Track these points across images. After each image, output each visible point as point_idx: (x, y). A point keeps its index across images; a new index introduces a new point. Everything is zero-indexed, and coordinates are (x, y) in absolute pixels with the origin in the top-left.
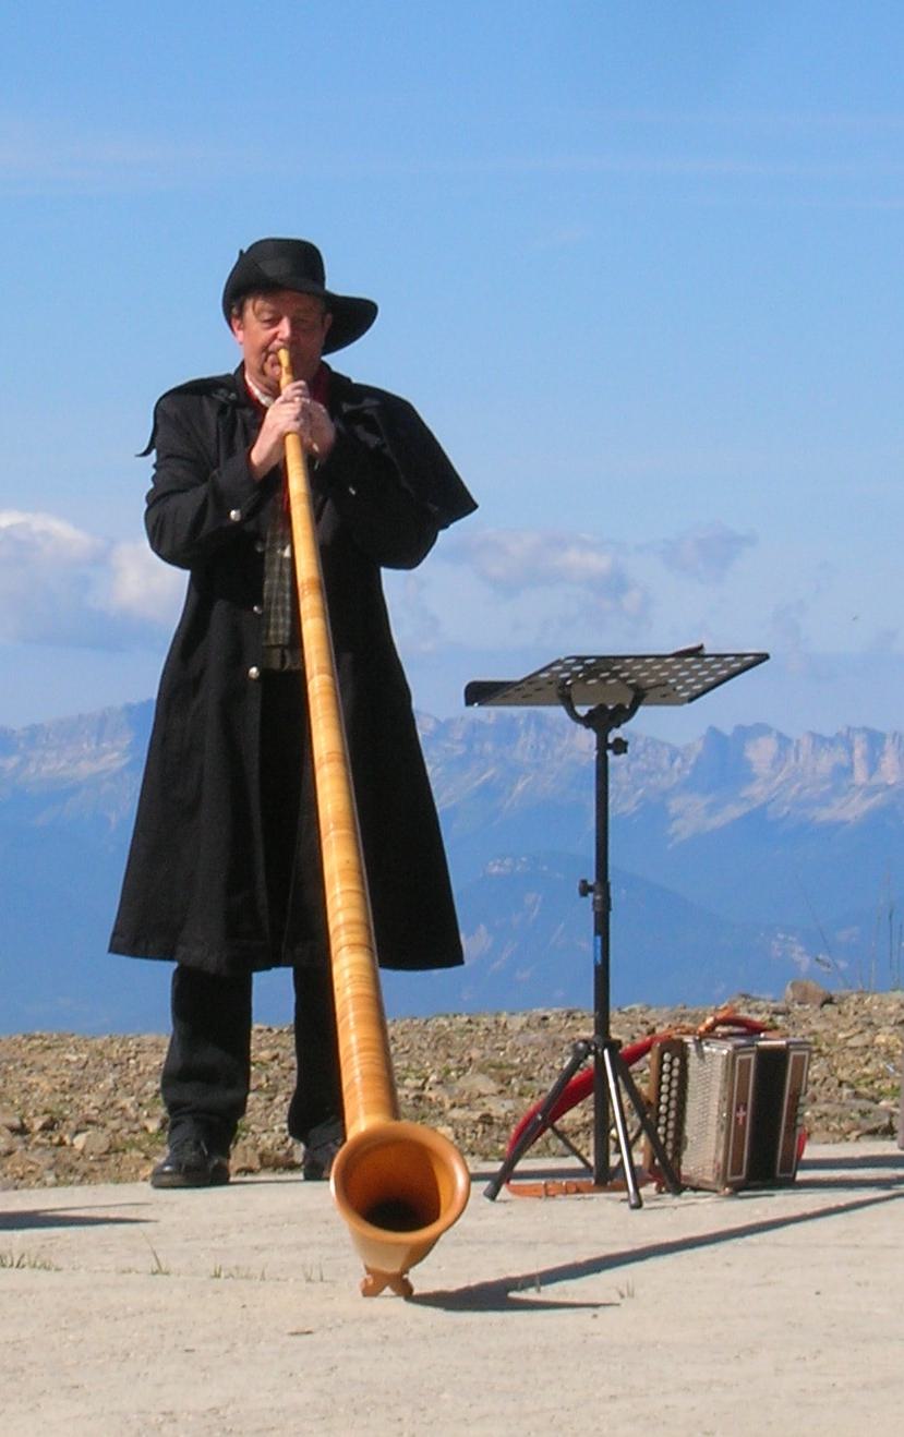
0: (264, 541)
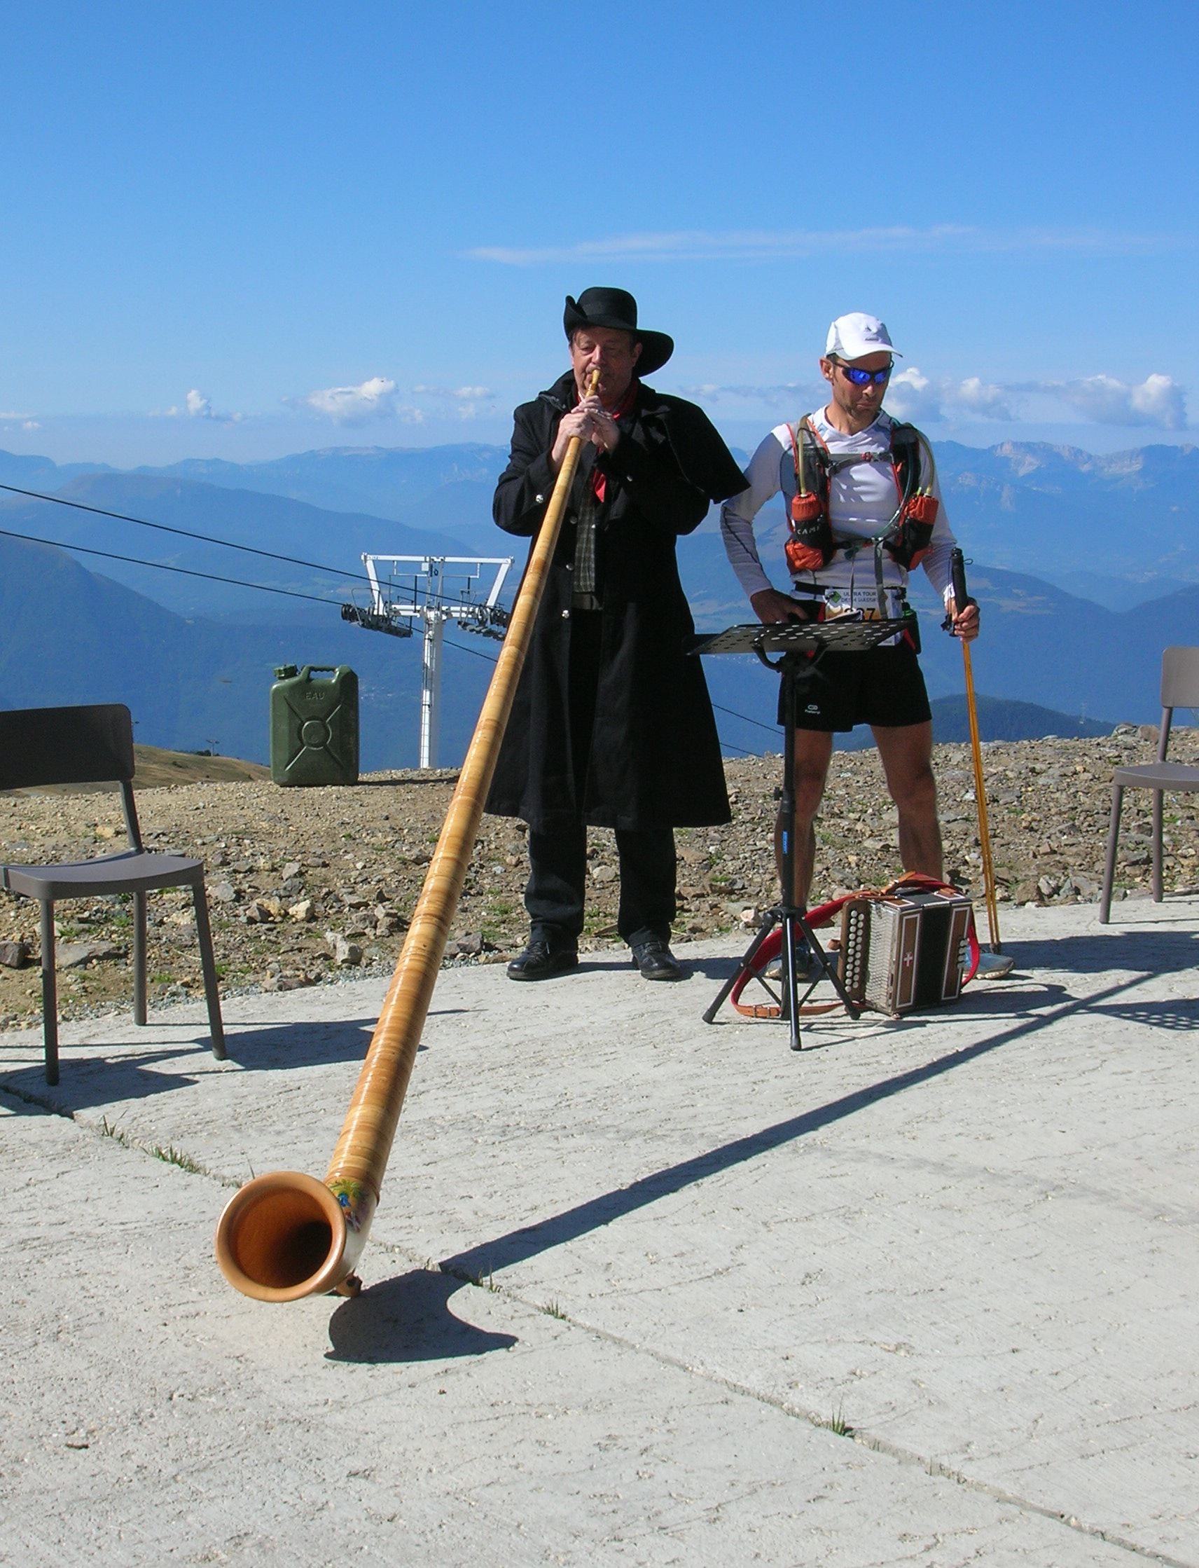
0: (577, 516)
